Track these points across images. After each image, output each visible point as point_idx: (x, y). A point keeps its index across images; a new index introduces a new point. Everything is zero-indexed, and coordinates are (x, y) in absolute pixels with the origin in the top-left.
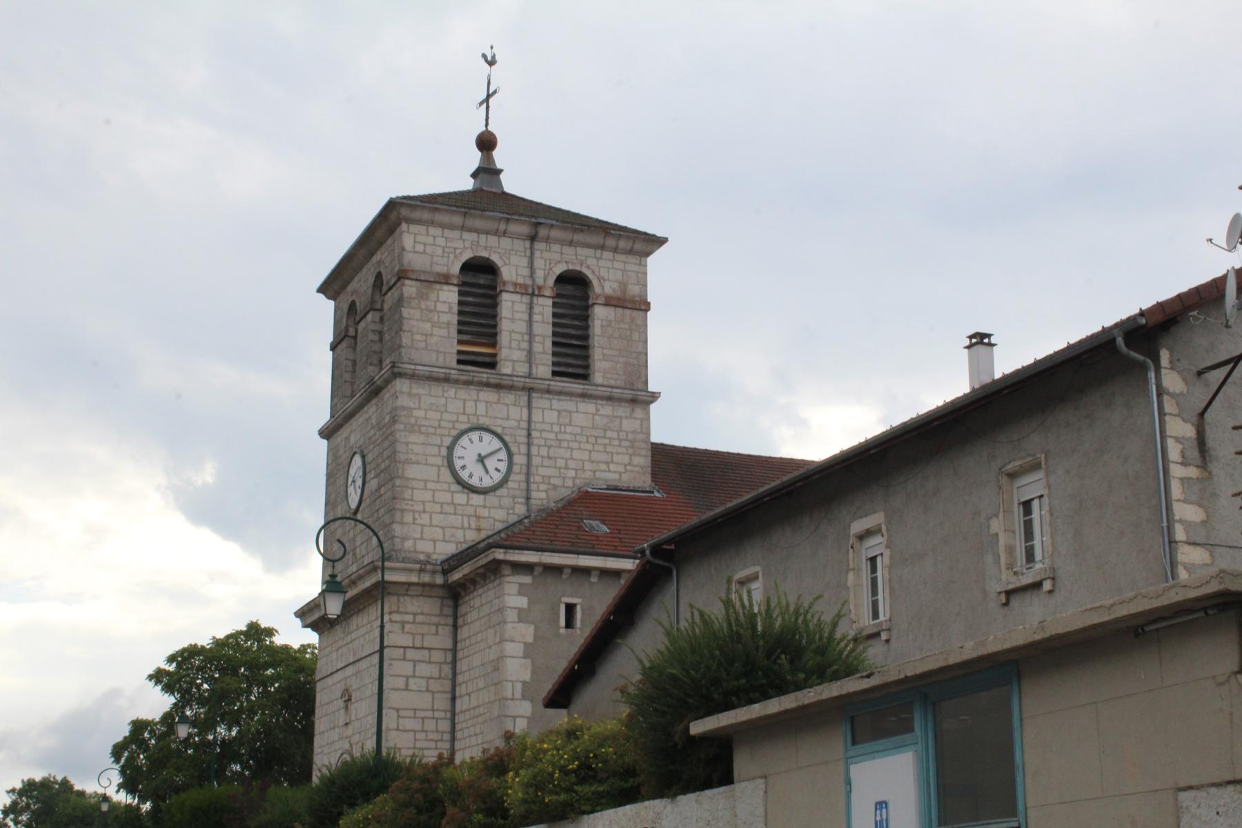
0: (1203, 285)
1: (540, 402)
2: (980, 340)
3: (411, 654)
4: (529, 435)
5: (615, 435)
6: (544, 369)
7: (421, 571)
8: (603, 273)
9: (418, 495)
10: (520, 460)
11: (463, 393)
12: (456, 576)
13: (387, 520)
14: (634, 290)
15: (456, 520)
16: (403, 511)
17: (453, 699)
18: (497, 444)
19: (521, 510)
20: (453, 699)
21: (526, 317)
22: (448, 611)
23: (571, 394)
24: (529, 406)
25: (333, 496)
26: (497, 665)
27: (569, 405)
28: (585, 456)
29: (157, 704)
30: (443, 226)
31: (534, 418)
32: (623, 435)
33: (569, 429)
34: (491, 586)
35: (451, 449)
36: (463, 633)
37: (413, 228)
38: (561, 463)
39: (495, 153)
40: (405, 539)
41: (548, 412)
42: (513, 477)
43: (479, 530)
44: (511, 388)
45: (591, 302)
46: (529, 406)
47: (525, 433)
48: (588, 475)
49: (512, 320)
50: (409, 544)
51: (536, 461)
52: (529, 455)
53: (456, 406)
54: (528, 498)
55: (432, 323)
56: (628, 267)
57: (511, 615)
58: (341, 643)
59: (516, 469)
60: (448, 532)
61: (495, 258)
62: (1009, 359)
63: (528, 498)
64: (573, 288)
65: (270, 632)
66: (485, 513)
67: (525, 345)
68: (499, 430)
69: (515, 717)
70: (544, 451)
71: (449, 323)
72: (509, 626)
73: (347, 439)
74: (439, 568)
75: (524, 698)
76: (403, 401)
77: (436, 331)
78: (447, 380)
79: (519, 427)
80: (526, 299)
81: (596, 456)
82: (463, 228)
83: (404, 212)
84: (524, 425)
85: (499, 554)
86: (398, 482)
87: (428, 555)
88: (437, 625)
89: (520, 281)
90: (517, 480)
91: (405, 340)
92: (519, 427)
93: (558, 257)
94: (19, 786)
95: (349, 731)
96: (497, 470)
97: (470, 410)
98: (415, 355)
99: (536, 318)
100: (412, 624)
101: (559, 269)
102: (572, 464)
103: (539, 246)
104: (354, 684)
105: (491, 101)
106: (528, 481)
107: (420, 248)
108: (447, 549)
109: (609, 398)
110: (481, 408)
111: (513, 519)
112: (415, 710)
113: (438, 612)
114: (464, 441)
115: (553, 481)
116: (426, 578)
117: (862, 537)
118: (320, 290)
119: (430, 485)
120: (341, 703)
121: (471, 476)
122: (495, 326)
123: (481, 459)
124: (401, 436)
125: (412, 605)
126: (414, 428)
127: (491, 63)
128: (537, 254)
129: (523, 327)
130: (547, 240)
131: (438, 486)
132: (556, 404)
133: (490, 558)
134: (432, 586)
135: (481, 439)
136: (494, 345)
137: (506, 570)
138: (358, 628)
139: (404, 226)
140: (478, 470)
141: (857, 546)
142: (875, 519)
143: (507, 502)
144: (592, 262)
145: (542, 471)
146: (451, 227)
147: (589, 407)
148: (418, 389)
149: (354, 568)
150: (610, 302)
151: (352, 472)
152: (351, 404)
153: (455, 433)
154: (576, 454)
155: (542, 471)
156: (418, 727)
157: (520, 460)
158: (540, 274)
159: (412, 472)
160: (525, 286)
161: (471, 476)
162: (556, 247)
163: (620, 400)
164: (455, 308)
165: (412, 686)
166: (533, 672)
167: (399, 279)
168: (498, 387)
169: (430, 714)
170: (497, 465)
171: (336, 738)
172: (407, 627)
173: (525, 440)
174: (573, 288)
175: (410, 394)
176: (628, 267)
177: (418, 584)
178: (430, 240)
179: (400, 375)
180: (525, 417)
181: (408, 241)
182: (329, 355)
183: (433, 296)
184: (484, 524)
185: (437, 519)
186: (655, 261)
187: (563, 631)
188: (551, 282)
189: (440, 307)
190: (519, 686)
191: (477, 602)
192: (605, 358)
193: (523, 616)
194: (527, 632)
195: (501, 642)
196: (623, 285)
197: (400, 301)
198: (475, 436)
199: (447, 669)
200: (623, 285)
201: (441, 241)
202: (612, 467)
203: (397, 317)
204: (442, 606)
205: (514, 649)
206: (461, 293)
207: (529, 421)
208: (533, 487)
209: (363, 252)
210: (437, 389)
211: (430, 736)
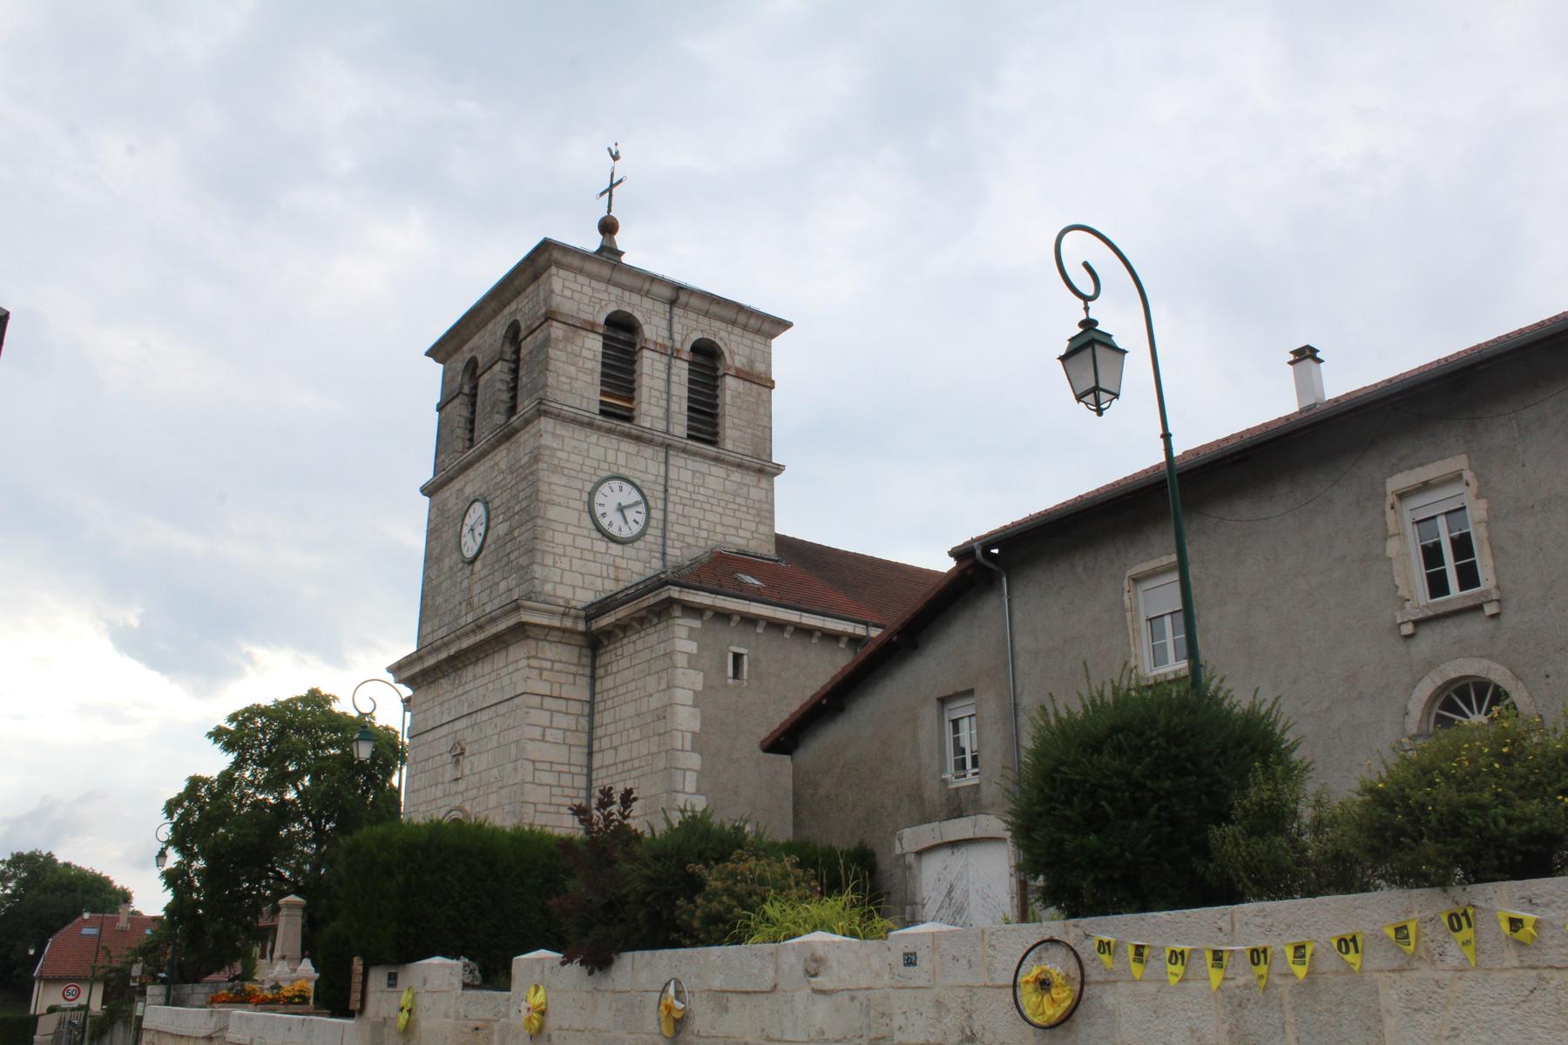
1: (677, 460)
2: (1305, 355)
3: (548, 703)
4: (666, 491)
5: (742, 501)
6: (680, 428)
7: (564, 615)
8: (734, 347)
9: (559, 538)
10: (657, 514)
11: (605, 441)
12: (605, 621)
13: (524, 561)
14: (760, 367)
15: (595, 568)
16: (544, 552)
17: (590, 754)
18: (636, 497)
19: (657, 564)
20: (590, 754)
21: (664, 376)
22: (586, 661)
23: (705, 456)
24: (666, 463)
25: (437, 551)
26: (663, 714)
27: (702, 466)
28: (716, 519)
29: (216, 762)
30: (590, 276)
31: (671, 475)
32: (750, 503)
33: (702, 490)
34: (651, 630)
35: (592, 494)
36: (606, 683)
37: (562, 273)
38: (695, 522)
39: (616, 237)
40: (545, 581)
41: (685, 470)
42: (650, 531)
43: (617, 580)
44: (650, 442)
45: (720, 373)
46: (666, 463)
47: (661, 488)
48: (719, 537)
49: (652, 377)
50: (548, 587)
51: (672, 517)
52: (665, 510)
53: (597, 452)
54: (664, 554)
55: (576, 370)
56: (756, 346)
57: (681, 660)
58: (446, 697)
59: (653, 523)
60: (588, 579)
61: (637, 315)
62: (1340, 381)
63: (664, 554)
64: (706, 357)
65: (327, 700)
66: (623, 563)
67: (663, 403)
68: (638, 482)
69: (684, 770)
70: (679, 509)
71: (593, 371)
72: (680, 671)
73: (461, 490)
74: (583, 613)
75: (693, 750)
76: (547, 440)
77: (580, 376)
78: (590, 425)
79: (656, 482)
80: (665, 359)
81: (726, 520)
82: (609, 282)
83: (556, 255)
84: (661, 480)
85: (675, 592)
86: (539, 522)
87: (567, 601)
88: (575, 675)
89: (660, 341)
90: (654, 532)
91: (551, 380)
92: (656, 482)
93: (694, 325)
94: (8, 858)
95: (461, 786)
97: (610, 458)
98: (560, 397)
99: (674, 378)
100: (536, 677)
101: (696, 336)
102: (704, 525)
103: (677, 311)
104: (469, 736)
105: (615, 190)
106: (664, 537)
107: (568, 293)
108: (586, 597)
109: (739, 466)
110: (622, 459)
111: (649, 573)
113: (575, 660)
114: (605, 488)
115: (688, 540)
116: (568, 623)
117: (1402, 496)
118: (428, 354)
119: (571, 529)
120: (448, 758)
121: (610, 524)
122: (632, 382)
123: (621, 509)
124: (545, 476)
125: (552, 651)
126: (557, 469)
127: (615, 157)
128: (676, 319)
129: (661, 385)
130: (685, 306)
131: (579, 531)
132: (691, 464)
133: (664, 595)
134: (572, 632)
136: (631, 400)
137: (677, 612)
138: (475, 678)
139: (554, 270)
140: (617, 519)
141: (1397, 505)
142: (1459, 462)
143: (644, 555)
144: (723, 334)
145: (677, 528)
146: (597, 278)
147: (719, 471)
148: (564, 431)
149: (470, 618)
150: (740, 375)
151: (469, 521)
152: (453, 463)
153: (596, 479)
154: (709, 516)
155: (677, 528)
156: (554, 782)
157: (657, 514)
158: (677, 337)
159: (553, 513)
160: (665, 347)
161: (610, 524)
162: (693, 316)
163: (748, 468)
164: (600, 358)
165: (548, 738)
166: (703, 724)
167: (547, 319)
168: (638, 439)
169: (565, 768)
170: (636, 516)
171: (439, 794)
172: (545, 674)
173: (661, 495)
174: (706, 357)
175: (554, 434)
176: (756, 346)
177: (558, 629)
178: (578, 287)
179: (546, 413)
180: (662, 473)
181: (557, 284)
182: (435, 416)
183: (579, 342)
184: (623, 575)
185: (577, 564)
186: (779, 344)
187: (730, 681)
188: (688, 347)
189: (585, 353)
190: (689, 736)
191: (629, 649)
192: (735, 427)
193: (693, 662)
194: (697, 679)
195: (668, 688)
196: (751, 362)
197: (546, 342)
198: (615, 484)
199: (584, 722)
200: (751, 362)
201: (587, 290)
202: (741, 533)
203: (541, 358)
204: (580, 656)
205: (683, 696)
206: (605, 346)
207: (666, 478)
208: (669, 543)
209: (493, 304)
210: (580, 433)
211: (568, 792)
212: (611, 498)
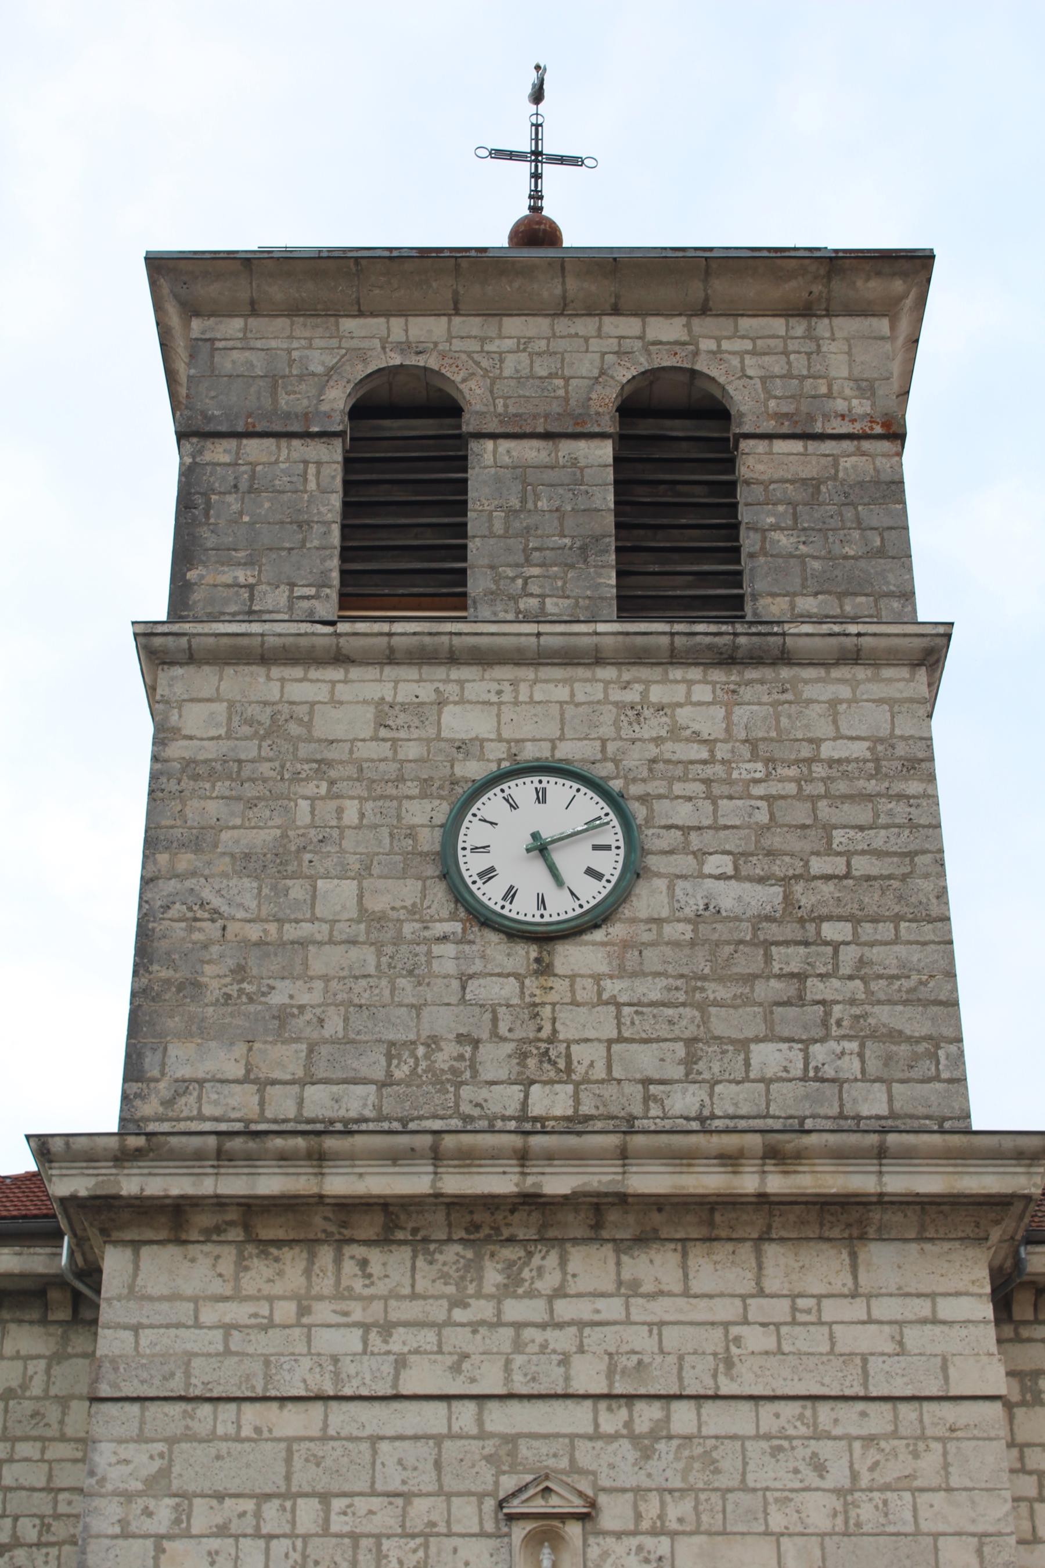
0: (903, 491)
96: (590, 872)
112: (935, 1321)
121: (510, 894)
135: (541, 797)
140: (532, 879)
198: (523, 789)
212: (505, 846)
